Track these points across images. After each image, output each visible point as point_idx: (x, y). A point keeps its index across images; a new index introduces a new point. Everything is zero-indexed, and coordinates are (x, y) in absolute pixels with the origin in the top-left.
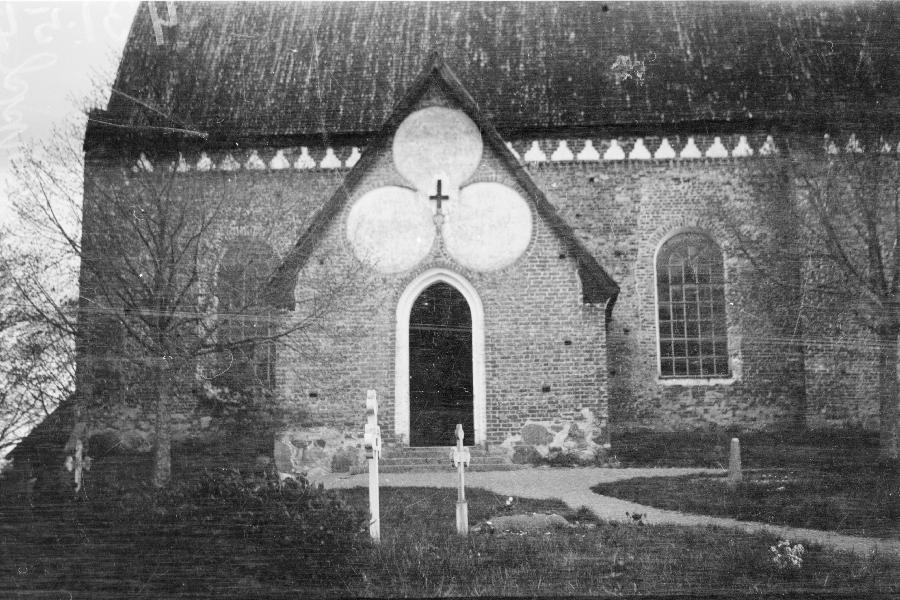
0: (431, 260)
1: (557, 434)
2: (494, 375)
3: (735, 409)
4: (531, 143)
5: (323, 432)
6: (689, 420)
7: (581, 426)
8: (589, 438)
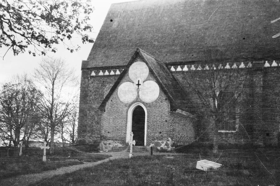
0: (136, 100)
1: (162, 144)
4: (185, 66)
5: (110, 141)
7: (168, 142)
8: (170, 145)
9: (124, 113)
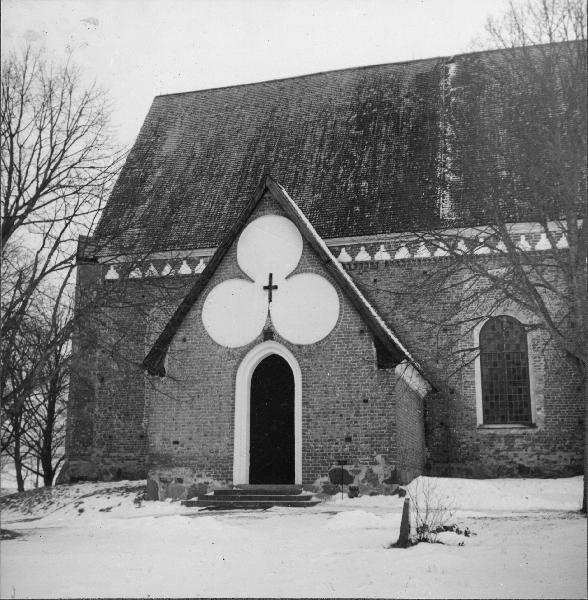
2: (309, 427)
3: (539, 454)
5: (180, 472)
7: (376, 469)
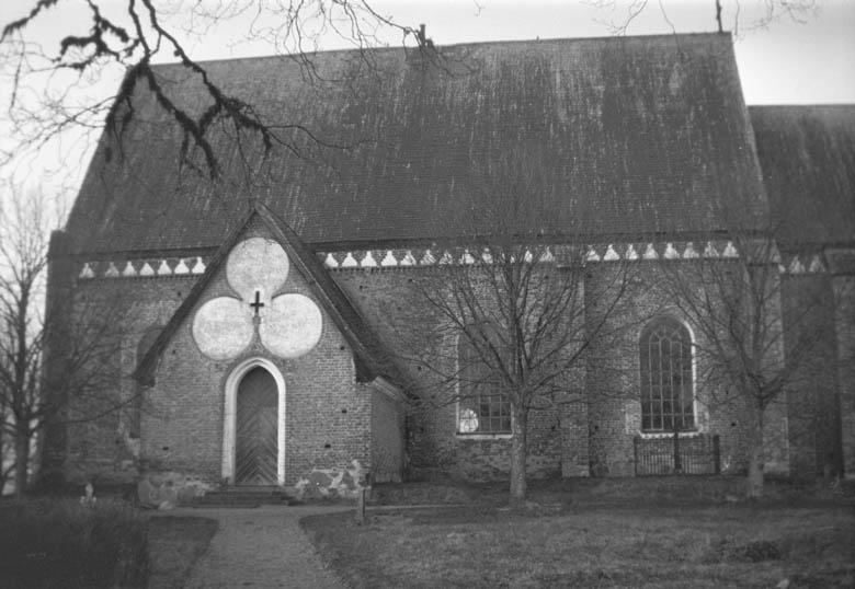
6: (478, 466)
7: (351, 473)
8: (356, 482)
9: (215, 390)
